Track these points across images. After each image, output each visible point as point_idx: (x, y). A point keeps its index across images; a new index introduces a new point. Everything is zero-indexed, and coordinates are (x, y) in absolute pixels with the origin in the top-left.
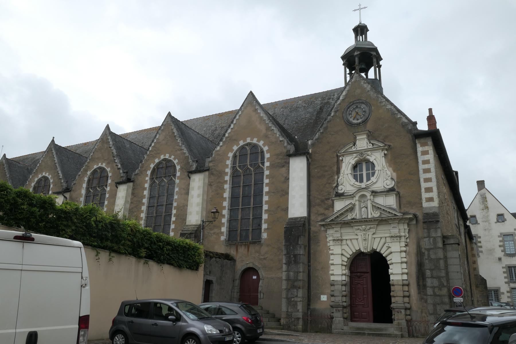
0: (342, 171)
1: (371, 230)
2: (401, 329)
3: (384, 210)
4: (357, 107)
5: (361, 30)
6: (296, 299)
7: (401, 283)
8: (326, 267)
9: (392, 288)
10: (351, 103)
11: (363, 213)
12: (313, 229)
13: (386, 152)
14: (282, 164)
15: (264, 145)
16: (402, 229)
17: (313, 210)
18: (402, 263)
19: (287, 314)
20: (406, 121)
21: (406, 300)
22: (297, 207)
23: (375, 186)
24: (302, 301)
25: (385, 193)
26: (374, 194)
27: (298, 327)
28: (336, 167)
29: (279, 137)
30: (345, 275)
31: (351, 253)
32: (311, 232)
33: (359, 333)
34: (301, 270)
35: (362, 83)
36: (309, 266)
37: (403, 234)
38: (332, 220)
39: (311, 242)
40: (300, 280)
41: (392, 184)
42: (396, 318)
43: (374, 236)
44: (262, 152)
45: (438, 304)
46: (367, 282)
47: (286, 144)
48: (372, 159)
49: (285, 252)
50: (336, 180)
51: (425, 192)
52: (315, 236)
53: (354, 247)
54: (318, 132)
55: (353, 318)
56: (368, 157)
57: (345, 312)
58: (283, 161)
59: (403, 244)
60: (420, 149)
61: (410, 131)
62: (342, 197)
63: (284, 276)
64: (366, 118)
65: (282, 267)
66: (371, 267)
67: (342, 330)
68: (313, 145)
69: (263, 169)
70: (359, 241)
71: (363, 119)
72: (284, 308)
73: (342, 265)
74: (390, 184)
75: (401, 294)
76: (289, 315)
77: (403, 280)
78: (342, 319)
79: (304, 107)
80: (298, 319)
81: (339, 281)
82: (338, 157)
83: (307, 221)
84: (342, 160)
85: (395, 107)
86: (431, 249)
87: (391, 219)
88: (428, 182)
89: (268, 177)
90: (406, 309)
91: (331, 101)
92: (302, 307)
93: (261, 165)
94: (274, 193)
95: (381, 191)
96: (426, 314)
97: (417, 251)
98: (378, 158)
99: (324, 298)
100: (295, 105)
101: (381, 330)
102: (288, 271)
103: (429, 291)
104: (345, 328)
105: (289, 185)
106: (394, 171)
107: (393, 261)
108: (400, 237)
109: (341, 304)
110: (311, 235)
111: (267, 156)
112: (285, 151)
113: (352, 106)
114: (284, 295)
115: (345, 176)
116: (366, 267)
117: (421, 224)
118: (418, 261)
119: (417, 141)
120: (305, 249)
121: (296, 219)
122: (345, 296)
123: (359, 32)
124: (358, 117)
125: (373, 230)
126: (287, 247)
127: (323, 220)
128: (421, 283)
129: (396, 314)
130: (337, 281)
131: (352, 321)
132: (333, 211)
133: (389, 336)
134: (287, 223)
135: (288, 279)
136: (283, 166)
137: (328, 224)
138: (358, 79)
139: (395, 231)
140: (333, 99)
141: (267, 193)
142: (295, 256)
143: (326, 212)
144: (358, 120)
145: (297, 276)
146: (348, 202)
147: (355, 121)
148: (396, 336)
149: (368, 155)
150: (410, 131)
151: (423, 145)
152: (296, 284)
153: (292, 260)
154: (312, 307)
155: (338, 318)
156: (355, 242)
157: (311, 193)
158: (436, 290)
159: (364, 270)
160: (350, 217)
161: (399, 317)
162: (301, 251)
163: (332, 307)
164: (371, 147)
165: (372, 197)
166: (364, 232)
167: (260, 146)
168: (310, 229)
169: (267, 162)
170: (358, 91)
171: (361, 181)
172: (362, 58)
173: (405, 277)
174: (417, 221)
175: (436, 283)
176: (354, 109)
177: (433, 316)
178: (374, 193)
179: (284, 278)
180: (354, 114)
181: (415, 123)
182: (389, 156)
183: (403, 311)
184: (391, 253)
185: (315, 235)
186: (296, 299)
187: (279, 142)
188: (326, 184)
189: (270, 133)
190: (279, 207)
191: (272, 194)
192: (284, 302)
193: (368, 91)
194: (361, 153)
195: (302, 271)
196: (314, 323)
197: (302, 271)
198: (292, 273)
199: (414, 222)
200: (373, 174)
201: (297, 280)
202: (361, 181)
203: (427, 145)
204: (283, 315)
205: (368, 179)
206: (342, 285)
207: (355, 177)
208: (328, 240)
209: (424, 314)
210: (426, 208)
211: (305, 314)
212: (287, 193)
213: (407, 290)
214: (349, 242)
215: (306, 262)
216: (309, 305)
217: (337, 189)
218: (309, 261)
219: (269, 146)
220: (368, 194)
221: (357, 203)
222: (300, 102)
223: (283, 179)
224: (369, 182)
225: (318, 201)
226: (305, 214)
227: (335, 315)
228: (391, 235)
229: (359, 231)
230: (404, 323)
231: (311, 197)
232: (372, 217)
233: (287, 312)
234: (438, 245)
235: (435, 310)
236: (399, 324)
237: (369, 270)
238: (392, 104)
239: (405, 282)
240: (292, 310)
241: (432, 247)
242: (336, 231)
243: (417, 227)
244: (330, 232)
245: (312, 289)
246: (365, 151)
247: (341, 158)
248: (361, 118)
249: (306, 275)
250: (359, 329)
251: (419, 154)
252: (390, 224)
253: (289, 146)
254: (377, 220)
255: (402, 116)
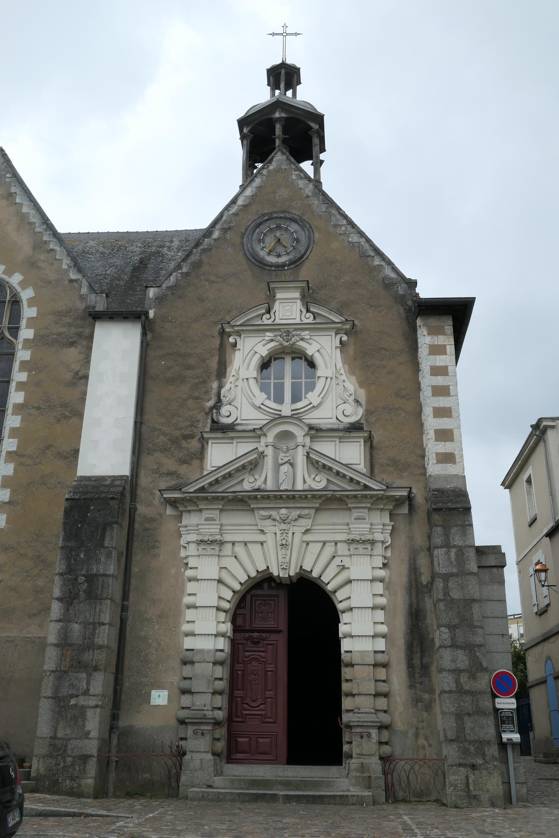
0: (232, 371)
1: (302, 522)
2: (368, 783)
3: (338, 473)
4: (279, 227)
5: (284, 76)
6: (82, 701)
7: (370, 660)
8: (172, 614)
9: (346, 673)
10: (264, 215)
11: (282, 477)
12: (142, 509)
13: (345, 338)
14: (76, 333)
15: (24, 284)
16: (376, 524)
17: (148, 461)
18: (374, 608)
19: (53, 746)
20: (393, 275)
21: (382, 703)
22: (105, 447)
23: (316, 414)
24: (102, 707)
25: (341, 434)
26: (313, 432)
27: (83, 782)
28: (216, 359)
29: (67, 271)
30: (223, 635)
31: (243, 578)
32: (138, 519)
33: (259, 796)
34: (106, 618)
35: (294, 177)
36: (124, 609)
37: (378, 536)
38: (202, 489)
39: (136, 544)
40: (100, 647)
41: (356, 413)
42: (355, 751)
43: (307, 538)
44: (16, 302)
45: (469, 715)
46: (274, 657)
47: (84, 290)
48: (310, 350)
49: (59, 566)
50: (214, 391)
51: (436, 440)
52: (146, 530)
53: (253, 562)
54: (175, 270)
55: (233, 751)
56: (302, 344)
57: (217, 736)
58: (73, 330)
59: (379, 561)
60: (425, 340)
61: (400, 300)
62: (231, 434)
63: (52, 633)
64: (298, 255)
65: (49, 608)
66: (293, 619)
67: (210, 786)
68: (160, 300)
69: (12, 346)
70: (267, 548)
71: (291, 256)
72: (44, 729)
73: (218, 609)
74: (355, 414)
75: (370, 688)
76: (57, 748)
77: (376, 652)
78: (210, 756)
79: (103, 253)
80: (85, 758)
81: (209, 651)
82: (223, 334)
83: (128, 488)
84: (235, 345)
85: (368, 241)
86: (453, 575)
87: (355, 497)
88: (443, 417)
89: (24, 365)
90: (382, 727)
91: (165, 250)
92: (101, 722)
93: (7, 334)
94: (38, 408)
95: (330, 426)
96: (427, 739)
97: (410, 581)
98: (325, 349)
99: (159, 697)
100: (80, 248)
101: (316, 784)
102: (65, 620)
103: (443, 681)
104: (218, 781)
105: (85, 393)
106: (361, 384)
107: (353, 603)
108: (373, 542)
109: (209, 714)
110: (137, 526)
111: (29, 312)
112: (81, 306)
113: (268, 223)
114: (47, 689)
115: (240, 383)
116: (277, 616)
117: (421, 515)
118: (411, 605)
119: (419, 322)
120: (119, 561)
121: (100, 479)
122: (220, 693)
123: (283, 77)
124: (280, 249)
125: (306, 523)
126: (69, 553)
127: (178, 488)
128: (417, 661)
129: (356, 740)
130: (201, 651)
131: (230, 760)
132: (202, 468)
133: (342, 800)
134: (75, 487)
135: (64, 643)
136: (72, 344)
137: (190, 500)
138: (283, 167)
139: (360, 529)
140: (169, 247)
141: (18, 408)
142: (91, 578)
143: (183, 469)
144: (279, 256)
145: (93, 634)
146: (243, 448)
147: (272, 259)
148: (360, 802)
149: (302, 339)
150: (400, 300)
151: (433, 332)
152: (87, 657)
153: (81, 589)
154: (122, 723)
155: (200, 752)
156: (255, 549)
157: (146, 417)
158: (464, 678)
159: (270, 624)
160: (248, 484)
161: (362, 750)
162: (110, 567)
163: (182, 722)
164: (311, 320)
165: (308, 439)
166: (283, 526)
167: (11, 288)
168: (136, 509)
169: (28, 327)
170: (283, 193)
171: (279, 399)
172: (282, 133)
173: (381, 645)
174: (411, 507)
175: (462, 660)
176: (271, 230)
177: (455, 746)
178: (315, 432)
179: (52, 639)
180: (270, 241)
181: (413, 284)
182: (351, 350)
183: (374, 733)
184: (350, 581)
185: (147, 525)
186: (82, 701)
187: (66, 282)
188: (186, 400)
189: (43, 257)
190: (48, 447)
191: (33, 411)
192: (45, 708)
193: (308, 197)
194: (286, 330)
195: (107, 620)
196: (135, 771)
197: (107, 620)
198: (76, 627)
199: (405, 510)
200: (311, 387)
201: (90, 645)
202: (279, 399)
203: (444, 334)
204: (41, 748)
205: (296, 398)
206: (215, 664)
207: (264, 388)
208: (182, 542)
209: (422, 741)
210: (438, 477)
211: (105, 743)
212: (80, 415)
213: (384, 678)
214: (240, 550)
215: (118, 598)
216: (114, 717)
217: (218, 413)
218: (125, 596)
219: (36, 288)
220: (299, 433)
221: (269, 452)
222: (91, 243)
223: (68, 376)
224: (299, 405)
225: (162, 440)
226: (125, 470)
227: (189, 745)
228: (351, 537)
229: (269, 522)
230: (375, 764)
231: (144, 429)
232: (306, 487)
233: (54, 738)
234: (467, 566)
235: (461, 729)
236: (363, 768)
237: (283, 625)
238: (361, 234)
239: (381, 658)
240: (68, 731)
241: (455, 570)
242: (207, 519)
243: (411, 522)
244: (191, 520)
245: (126, 672)
246: (296, 329)
247: (231, 340)
248: (288, 254)
249: (115, 632)
250: (254, 783)
251: (423, 351)
252: (350, 509)
253: (93, 297)
254: (320, 497)
255: (383, 263)
